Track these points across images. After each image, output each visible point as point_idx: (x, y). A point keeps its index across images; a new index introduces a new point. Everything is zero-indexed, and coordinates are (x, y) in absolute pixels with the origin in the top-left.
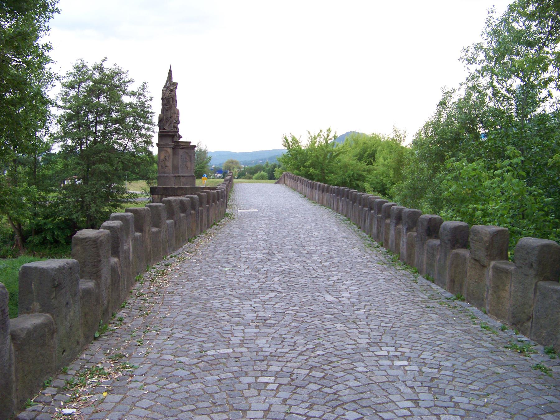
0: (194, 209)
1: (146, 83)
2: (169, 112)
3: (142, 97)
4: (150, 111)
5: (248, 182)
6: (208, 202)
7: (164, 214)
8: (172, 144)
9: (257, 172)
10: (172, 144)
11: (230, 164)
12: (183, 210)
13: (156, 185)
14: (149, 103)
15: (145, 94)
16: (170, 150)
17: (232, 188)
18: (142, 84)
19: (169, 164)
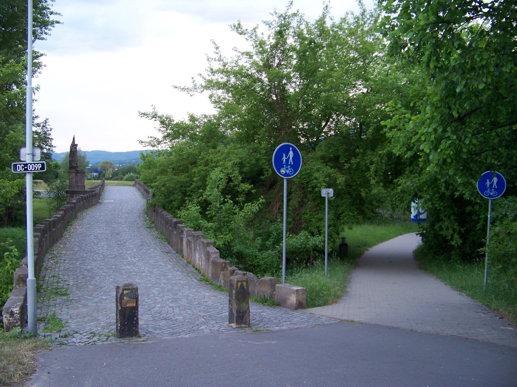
0: (88, 199)
1: (47, 119)
2: (74, 158)
3: (45, 128)
4: (50, 137)
5: (118, 185)
6: (92, 197)
7: (81, 200)
8: (75, 172)
9: (127, 174)
10: (75, 172)
11: (105, 165)
12: (85, 199)
13: (68, 190)
14: (50, 132)
15: (47, 126)
16: (74, 174)
17: (103, 189)
18: (45, 119)
19: (74, 180)
